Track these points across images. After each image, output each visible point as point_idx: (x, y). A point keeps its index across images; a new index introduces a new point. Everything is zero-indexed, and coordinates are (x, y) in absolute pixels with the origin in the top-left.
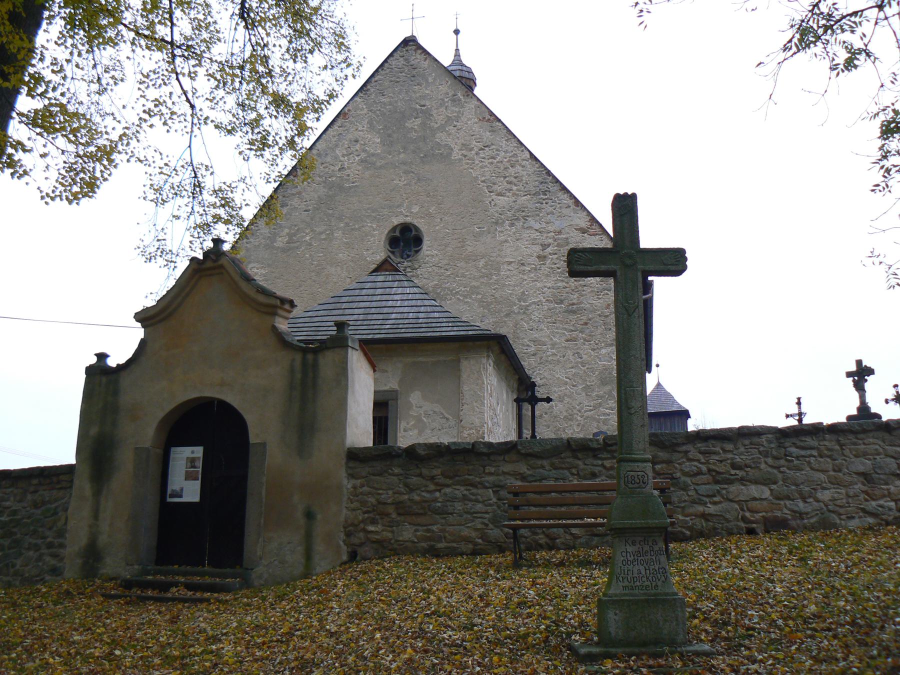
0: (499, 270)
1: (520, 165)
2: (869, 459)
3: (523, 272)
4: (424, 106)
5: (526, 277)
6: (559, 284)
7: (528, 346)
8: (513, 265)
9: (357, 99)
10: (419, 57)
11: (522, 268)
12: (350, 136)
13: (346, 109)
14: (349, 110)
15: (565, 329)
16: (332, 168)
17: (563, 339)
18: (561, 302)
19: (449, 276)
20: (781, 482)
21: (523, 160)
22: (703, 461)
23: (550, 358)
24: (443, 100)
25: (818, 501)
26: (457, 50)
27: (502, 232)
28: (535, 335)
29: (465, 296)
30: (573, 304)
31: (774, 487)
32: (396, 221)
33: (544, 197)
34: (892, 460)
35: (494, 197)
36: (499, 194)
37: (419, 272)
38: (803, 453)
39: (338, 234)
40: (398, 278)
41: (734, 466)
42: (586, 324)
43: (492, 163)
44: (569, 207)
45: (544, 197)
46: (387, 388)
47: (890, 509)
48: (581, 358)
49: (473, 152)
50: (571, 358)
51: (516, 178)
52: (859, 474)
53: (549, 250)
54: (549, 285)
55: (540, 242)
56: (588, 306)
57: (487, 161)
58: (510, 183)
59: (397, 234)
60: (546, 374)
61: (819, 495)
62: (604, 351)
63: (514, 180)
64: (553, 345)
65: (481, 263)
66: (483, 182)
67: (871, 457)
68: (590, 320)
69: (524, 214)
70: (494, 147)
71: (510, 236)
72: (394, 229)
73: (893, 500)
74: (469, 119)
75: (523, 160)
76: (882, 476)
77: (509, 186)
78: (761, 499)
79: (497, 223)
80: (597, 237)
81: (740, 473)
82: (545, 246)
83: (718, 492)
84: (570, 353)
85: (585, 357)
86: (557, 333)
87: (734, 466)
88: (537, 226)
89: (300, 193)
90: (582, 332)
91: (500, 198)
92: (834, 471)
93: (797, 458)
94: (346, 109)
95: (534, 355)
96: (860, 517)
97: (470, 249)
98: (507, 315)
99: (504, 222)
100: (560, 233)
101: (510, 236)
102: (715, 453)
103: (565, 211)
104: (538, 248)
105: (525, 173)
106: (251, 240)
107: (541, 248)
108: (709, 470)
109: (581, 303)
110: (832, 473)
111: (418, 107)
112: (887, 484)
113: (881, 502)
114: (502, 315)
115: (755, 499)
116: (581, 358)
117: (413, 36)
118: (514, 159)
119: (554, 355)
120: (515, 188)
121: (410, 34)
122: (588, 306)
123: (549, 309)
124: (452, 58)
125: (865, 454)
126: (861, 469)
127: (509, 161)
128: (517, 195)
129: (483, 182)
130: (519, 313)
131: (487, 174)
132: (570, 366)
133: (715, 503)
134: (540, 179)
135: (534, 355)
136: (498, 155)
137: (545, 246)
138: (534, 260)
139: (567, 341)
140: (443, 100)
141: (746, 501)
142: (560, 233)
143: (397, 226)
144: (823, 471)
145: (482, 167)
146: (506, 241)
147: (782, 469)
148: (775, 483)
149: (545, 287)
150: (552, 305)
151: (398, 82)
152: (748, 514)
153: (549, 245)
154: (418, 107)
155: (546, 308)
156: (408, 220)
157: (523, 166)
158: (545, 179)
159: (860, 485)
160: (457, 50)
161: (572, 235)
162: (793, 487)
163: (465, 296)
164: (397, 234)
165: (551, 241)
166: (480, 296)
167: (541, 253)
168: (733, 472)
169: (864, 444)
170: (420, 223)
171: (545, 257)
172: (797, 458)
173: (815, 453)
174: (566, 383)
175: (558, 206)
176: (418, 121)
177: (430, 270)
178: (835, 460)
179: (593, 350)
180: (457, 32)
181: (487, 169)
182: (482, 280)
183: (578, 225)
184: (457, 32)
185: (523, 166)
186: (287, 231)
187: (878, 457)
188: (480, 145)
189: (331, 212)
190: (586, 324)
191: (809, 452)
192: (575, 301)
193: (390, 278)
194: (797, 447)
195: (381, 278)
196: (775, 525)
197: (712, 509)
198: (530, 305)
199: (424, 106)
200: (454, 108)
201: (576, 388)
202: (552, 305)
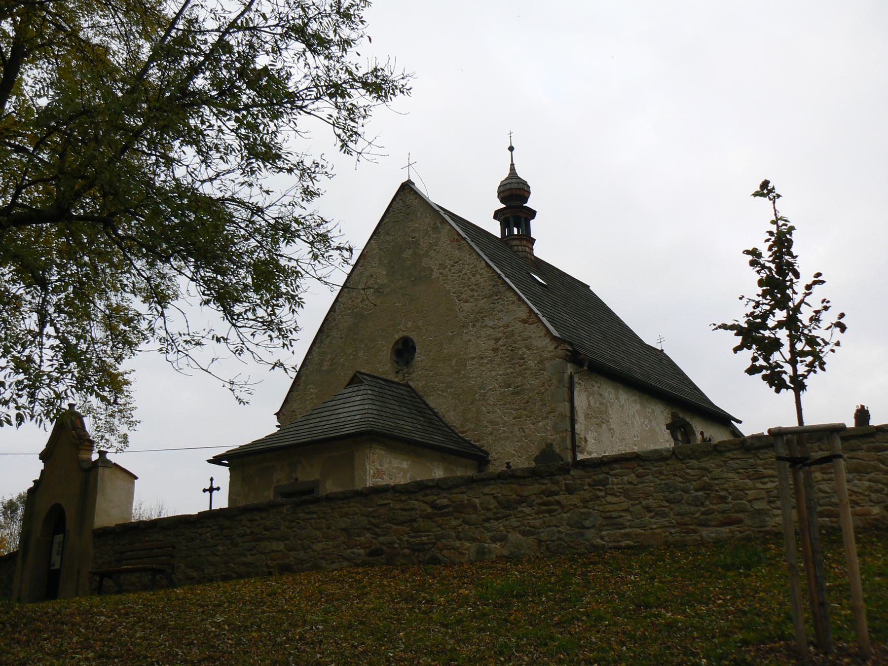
0: (465, 365)
1: (479, 274)
2: (349, 519)
3: (482, 365)
4: (414, 238)
5: (484, 369)
6: (509, 371)
7: (487, 427)
8: (475, 360)
9: (372, 241)
10: (411, 197)
11: (482, 361)
12: (367, 273)
13: (365, 252)
14: (367, 252)
15: (512, 409)
16: (356, 300)
17: (511, 418)
18: (509, 386)
19: (432, 376)
20: (292, 538)
21: (481, 269)
22: (249, 526)
23: (502, 435)
24: (427, 229)
25: (313, 551)
26: (512, 165)
27: (467, 333)
28: (492, 417)
29: (443, 391)
30: (518, 387)
31: (286, 542)
32: (397, 337)
33: (496, 298)
34: (364, 517)
35: (462, 304)
36: (466, 301)
37: (413, 375)
38: (307, 516)
39: (361, 354)
40: (362, 388)
41: (266, 529)
42: (527, 402)
43: (460, 276)
44: (514, 302)
45: (496, 298)
46: (312, 479)
47: (359, 555)
48: (524, 432)
49: (447, 270)
50: (517, 433)
51: (476, 285)
52: (343, 529)
53: (500, 343)
54: (501, 372)
55: (494, 337)
56: (529, 386)
57: (456, 275)
58: (472, 290)
59: (400, 346)
60: (499, 449)
61: (314, 547)
62: (541, 424)
63: (474, 287)
64: (504, 424)
65: (454, 362)
66: (454, 293)
67: (351, 517)
68: (530, 398)
69: (482, 315)
70: (461, 262)
71: (472, 335)
72: (397, 342)
73: (362, 548)
74: (444, 242)
75: (481, 269)
76: (356, 531)
77: (471, 293)
78: (278, 551)
79: (463, 327)
80: (535, 325)
81: (268, 533)
82: (497, 340)
83: (255, 547)
84: (516, 429)
85: (527, 431)
86: (507, 413)
87: (266, 529)
88: (491, 324)
89: (336, 325)
90: (525, 410)
91: (467, 304)
92: (327, 528)
93: (304, 520)
94: (365, 252)
95: (491, 434)
96: (340, 562)
97: (446, 351)
98: (472, 403)
99: (468, 324)
100: (508, 326)
101: (472, 335)
102: (256, 520)
103: (511, 307)
104: (492, 343)
105: (482, 280)
106: (309, 367)
107: (494, 342)
108: (252, 533)
109: (524, 385)
110: (325, 530)
111: (411, 239)
112: (359, 536)
113: (355, 550)
114: (468, 403)
115: (273, 551)
116: (524, 432)
117: (409, 181)
118: (474, 270)
119: (505, 432)
120: (476, 294)
121: (406, 180)
122: (529, 386)
123: (501, 393)
124: (508, 172)
125: (346, 515)
126: (343, 525)
127: (471, 272)
128: (477, 300)
129: (454, 293)
130: (480, 399)
131: (456, 286)
132: (516, 440)
133: (252, 555)
134: (493, 283)
135: (491, 434)
136: (463, 268)
137: (497, 340)
138: (490, 353)
139: (514, 418)
140: (427, 229)
141: (269, 553)
142: (508, 326)
143: (399, 340)
144: (320, 529)
145: (453, 281)
146: (470, 340)
147: (294, 529)
148: (288, 539)
149: (498, 375)
150: (502, 390)
151: (397, 222)
152: (269, 562)
153: (500, 338)
154: (411, 239)
155: (498, 393)
156: (405, 334)
157: (481, 274)
158: (496, 282)
159: (342, 538)
160: (512, 165)
161: (516, 327)
162: (299, 542)
163: (443, 391)
164: (400, 346)
165: (501, 335)
166: (453, 390)
167: (495, 346)
168: (264, 533)
169: (348, 507)
170: (413, 336)
171: (497, 349)
172: (304, 520)
173: (315, 516)
174: (514, 455)
175: (506, 303)
176: (411, 252)
177: (420, 373)
178: (327, 520)
179: (533, 424)
180: (511, 149)
181: (456, 282)
182: (454, 376)
183: (520, 318)
184: (511, 149)
185: (481, 274)
186: (329, 356)
187: (355, 517)
188: (451, 263)
189: (356, 336)
190: (527, 402)
191: (310, 516)
192: (519, 384)
193: (356, 389)
194: (306, 513)
195: (350, 390)
196: (285, 569)
197: (250, 559)
198: (487, 392)
199: (414, 238)
200: (434, 236)
201: (521, 459)
202: (502, 390)
